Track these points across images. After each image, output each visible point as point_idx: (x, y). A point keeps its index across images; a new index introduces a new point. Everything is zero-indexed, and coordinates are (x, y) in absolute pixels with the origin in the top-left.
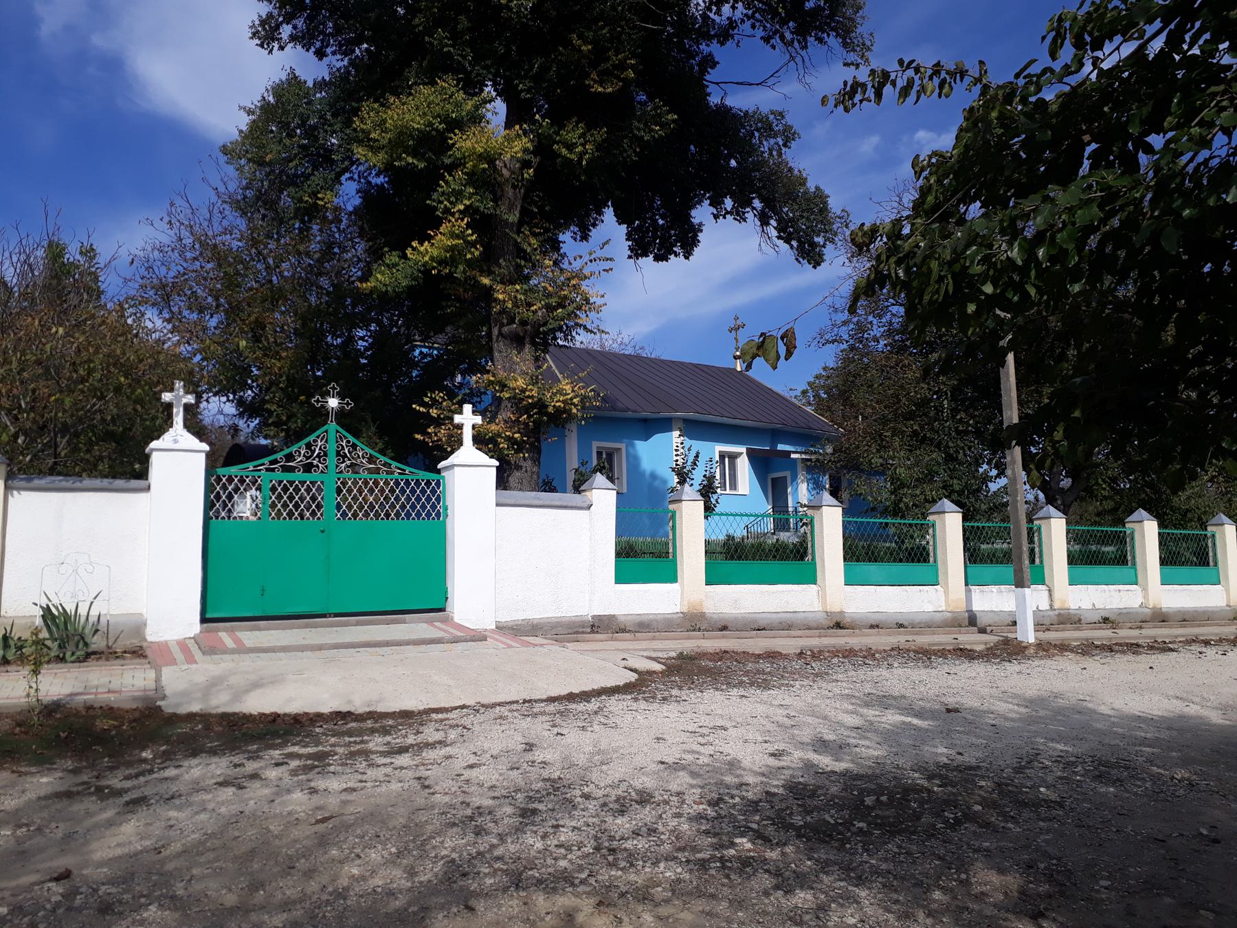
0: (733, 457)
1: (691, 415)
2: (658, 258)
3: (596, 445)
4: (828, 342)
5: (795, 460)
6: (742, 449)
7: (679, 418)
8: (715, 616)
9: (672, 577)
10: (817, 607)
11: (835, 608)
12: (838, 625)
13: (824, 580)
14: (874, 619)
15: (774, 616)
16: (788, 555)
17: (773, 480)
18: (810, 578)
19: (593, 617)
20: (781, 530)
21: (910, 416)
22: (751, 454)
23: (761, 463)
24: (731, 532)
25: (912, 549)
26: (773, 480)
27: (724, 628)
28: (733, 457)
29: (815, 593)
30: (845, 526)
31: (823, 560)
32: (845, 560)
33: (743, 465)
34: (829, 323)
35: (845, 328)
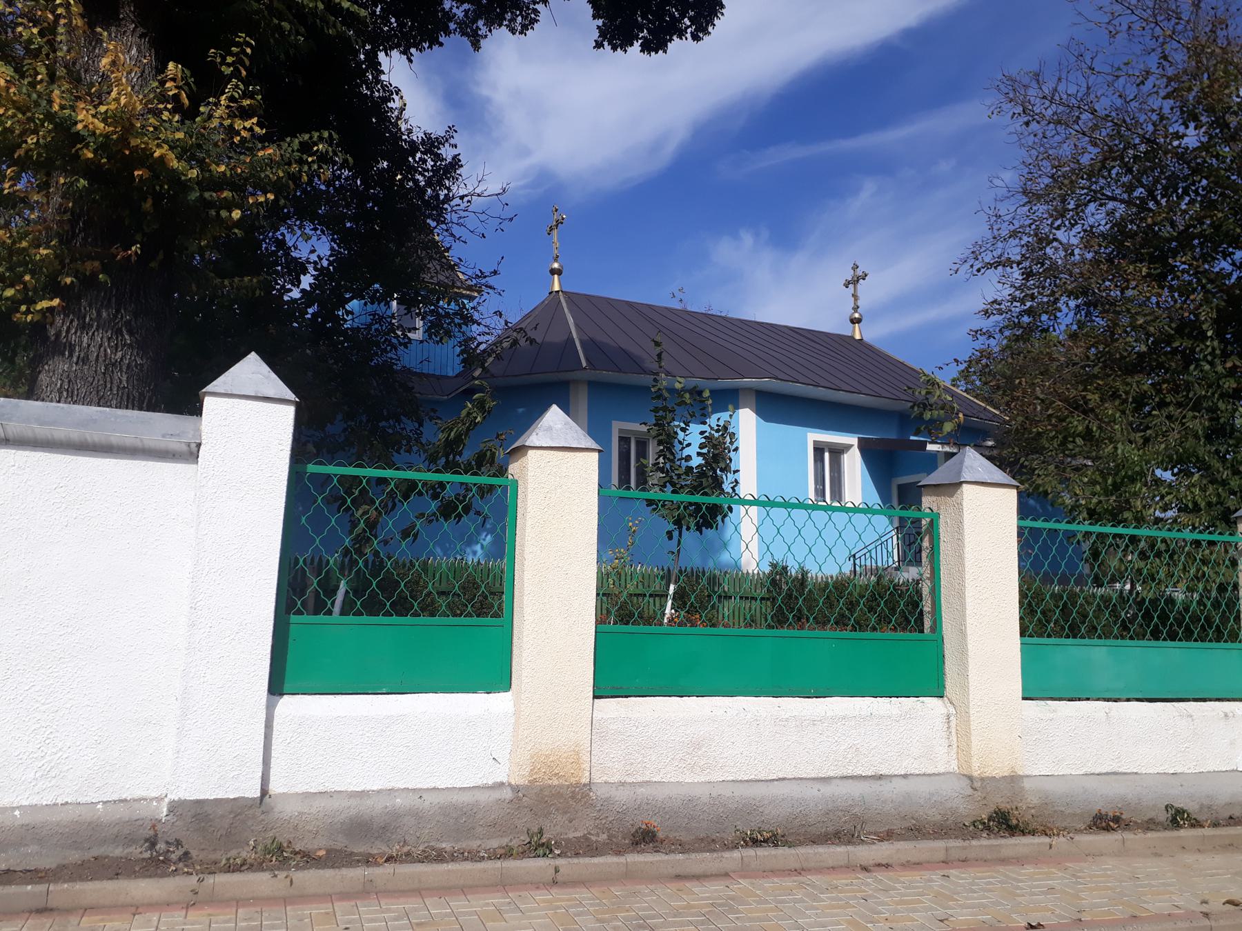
0: (837, 452)
1: (766, 383)
2: (647, 48)
3: (617, 427)
4: (989, 266)
5: (935, 455)
6: (852, 440)
7: (748, 390)
8: (622, 796)
9: (496, 677)
10: (944, 761)
11: (997, 767)
12: (1004, 822)
13: (965, 687)
14: (1106, 796)
15: (812, 792)
16: (877, 623)
17: (900, 487)
18: (926, 679)
19: (175, 807)
20: (910, 563)
21: (1138, 365)
22: (865, 447)
23: (881, 461)
24: (778, 557)
25: (1154, 602)
26: (900, 487)
27: (645, 838)
28: (837, 452)
29: (940, 723)
30: (1027, 540)
31: (962, 633)
32: (1023, 633)
33: (853, 463)
34: (989, 235)
35: (1013, 242)
